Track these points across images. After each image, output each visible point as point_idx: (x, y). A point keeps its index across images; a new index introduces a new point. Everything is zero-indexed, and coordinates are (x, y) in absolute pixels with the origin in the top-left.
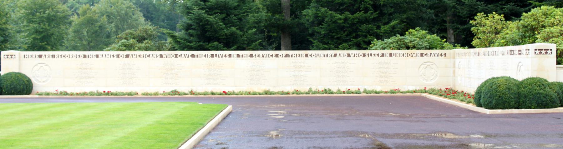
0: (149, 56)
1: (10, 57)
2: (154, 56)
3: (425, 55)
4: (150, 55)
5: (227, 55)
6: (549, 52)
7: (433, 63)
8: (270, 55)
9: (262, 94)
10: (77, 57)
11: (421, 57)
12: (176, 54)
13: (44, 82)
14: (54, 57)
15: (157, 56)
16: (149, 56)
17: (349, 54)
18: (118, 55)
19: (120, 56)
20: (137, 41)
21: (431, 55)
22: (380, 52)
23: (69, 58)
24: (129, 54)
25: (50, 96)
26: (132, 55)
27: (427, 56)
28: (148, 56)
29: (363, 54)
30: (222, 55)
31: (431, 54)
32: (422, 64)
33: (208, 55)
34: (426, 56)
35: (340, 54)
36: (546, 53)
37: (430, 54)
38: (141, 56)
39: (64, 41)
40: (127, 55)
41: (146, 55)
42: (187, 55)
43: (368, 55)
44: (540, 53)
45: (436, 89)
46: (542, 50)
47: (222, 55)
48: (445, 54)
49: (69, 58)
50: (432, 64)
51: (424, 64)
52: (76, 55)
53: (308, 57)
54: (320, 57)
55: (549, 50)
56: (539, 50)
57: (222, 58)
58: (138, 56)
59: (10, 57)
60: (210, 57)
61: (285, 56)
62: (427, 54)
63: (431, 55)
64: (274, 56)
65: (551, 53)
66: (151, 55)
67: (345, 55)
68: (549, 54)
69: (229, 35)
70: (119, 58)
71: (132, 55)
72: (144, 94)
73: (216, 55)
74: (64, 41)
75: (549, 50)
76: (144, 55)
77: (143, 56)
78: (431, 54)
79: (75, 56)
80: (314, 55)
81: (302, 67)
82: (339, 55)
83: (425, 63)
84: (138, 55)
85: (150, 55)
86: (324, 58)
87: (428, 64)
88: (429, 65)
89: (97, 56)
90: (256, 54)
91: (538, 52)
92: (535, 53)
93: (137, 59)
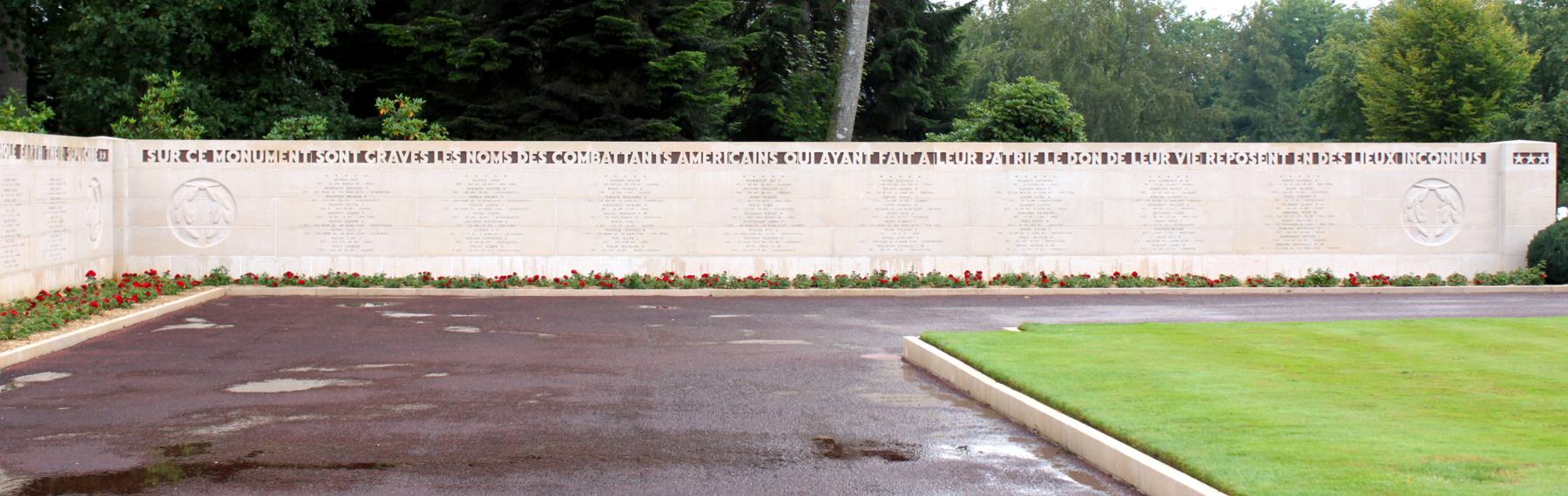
0: (739, 157)
1: (1531, 159)
2: (855, 155)
3: (371, 156)
4: (742, 154)
5: (541, 155)
6: (1543, 158)
7: (215, 181)
8: (731, 157)
9: (867, 286)
10: (1119, 161)
11: (1288, 165)
12: (184, 149)
13: (1438, 236)
14: (1204, 162)
15: (770, 159)
16: (739, 157)
17: (1174, 154)
18: (184, 153)
19: (786, 157)
20: (1339, 121)
21: (387, 158)
22: (972, 148)
23: (576, 162)
24: (920, 151)
25: (1362, 289)
26: (688, 154)
27: (198, 161)
28: (736, 157)
29: (977, 153)
30: (410, 153)
31: (388, 153)
32: (183, 185)
33: (1029, 154)
34: (374, 159)
35: (851, 154)
36: (1537, 161)
37: (385, 155)
38: (714, 156)
39: (61, 97)
40: (916, 153)
41: (1418, 154)
42: (1180, 154)
43: (953, 156)
44: (1525, 161)
45: (417, 276)
46: (1528, 154)
47: (410, 153)
48: (1483, 156)
49: (576, 162)
50: (217, 184)
51: (188, 184)
52: (528, 153)
53: (366, 162)
54: (264, 161)
55: (1543, 155)
56: (1522, 154)
57: (408, 164)
58: (704, 156)
59: (1531, 159)
60: (975, 162)
61: (1123, 158)
62: (376, 152)
63: (387, 158)
64: (201, 156)
65: (1547, 160)
66: (746, 155)
67: (1320, 158)
68: (1543, 163)
69: (296, 86)
70: (185, 163)
71: (688, 154)
72: (1251, 282)
73: (1138, 155)
74: (61, 97)
75: (1543, 155)
76: (723, 153)
77: (720, 156)
78: (388, 153)
79: (523, 157)
80: (570, 157)
81: (363, 195)
82: (686, 158)
83: (1419, 182)
84: (1284, 154)
85: (742, 154)
86: (351, 164)
87: (204, 184)
88: (1434, 190)
89: (1127, 158)
90: (157, 151)
91: (1519, 158)
92: (1515, 160)
93: (1216, 165)
